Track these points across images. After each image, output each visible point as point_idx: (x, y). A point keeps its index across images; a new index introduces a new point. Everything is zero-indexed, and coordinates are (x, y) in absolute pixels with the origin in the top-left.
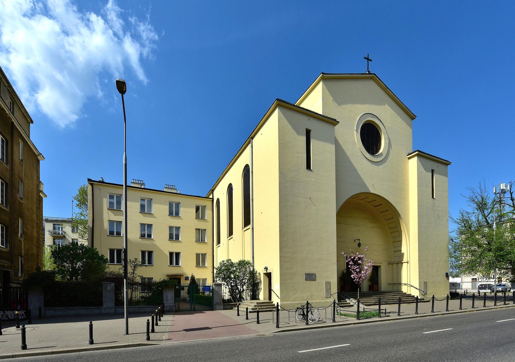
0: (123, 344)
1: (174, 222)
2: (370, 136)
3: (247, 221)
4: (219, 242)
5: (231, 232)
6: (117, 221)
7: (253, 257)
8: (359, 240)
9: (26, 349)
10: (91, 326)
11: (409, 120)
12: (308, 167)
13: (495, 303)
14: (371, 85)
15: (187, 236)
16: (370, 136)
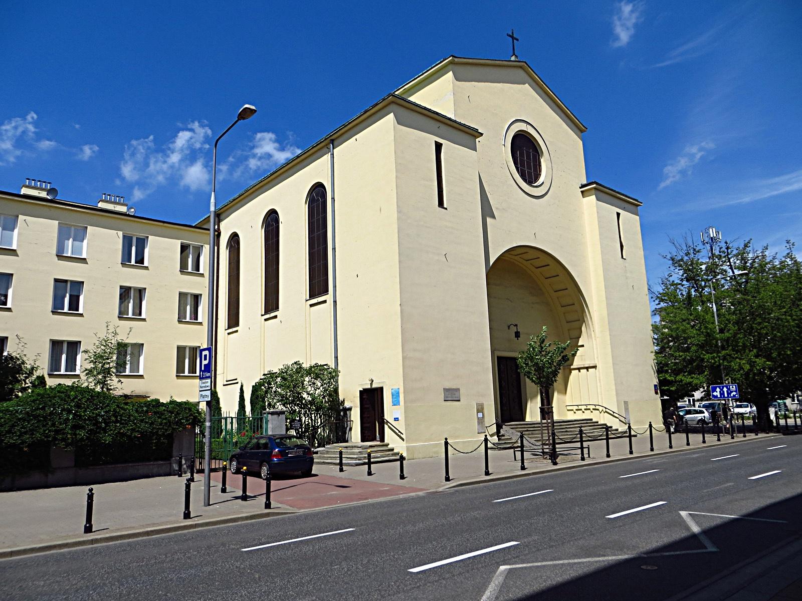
0: (616, 459)
1: (133, 278)
2: (526, 153)
3: (319, 283)
4: (234, 321)
5: (271, 303)
6: (72, 282)
7: (336, 358)
8: (516, 325)
9: (91, 531)
10: (90, 497)
11: (579, 133)
12: (441, 204)
13: (719, 436)
14: (521, 73)
15: (160, 307)
16: (526, 153)
